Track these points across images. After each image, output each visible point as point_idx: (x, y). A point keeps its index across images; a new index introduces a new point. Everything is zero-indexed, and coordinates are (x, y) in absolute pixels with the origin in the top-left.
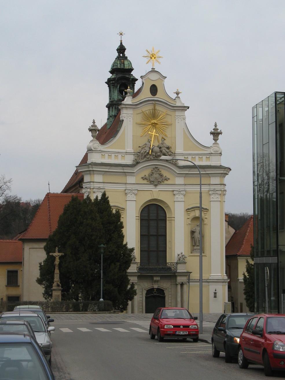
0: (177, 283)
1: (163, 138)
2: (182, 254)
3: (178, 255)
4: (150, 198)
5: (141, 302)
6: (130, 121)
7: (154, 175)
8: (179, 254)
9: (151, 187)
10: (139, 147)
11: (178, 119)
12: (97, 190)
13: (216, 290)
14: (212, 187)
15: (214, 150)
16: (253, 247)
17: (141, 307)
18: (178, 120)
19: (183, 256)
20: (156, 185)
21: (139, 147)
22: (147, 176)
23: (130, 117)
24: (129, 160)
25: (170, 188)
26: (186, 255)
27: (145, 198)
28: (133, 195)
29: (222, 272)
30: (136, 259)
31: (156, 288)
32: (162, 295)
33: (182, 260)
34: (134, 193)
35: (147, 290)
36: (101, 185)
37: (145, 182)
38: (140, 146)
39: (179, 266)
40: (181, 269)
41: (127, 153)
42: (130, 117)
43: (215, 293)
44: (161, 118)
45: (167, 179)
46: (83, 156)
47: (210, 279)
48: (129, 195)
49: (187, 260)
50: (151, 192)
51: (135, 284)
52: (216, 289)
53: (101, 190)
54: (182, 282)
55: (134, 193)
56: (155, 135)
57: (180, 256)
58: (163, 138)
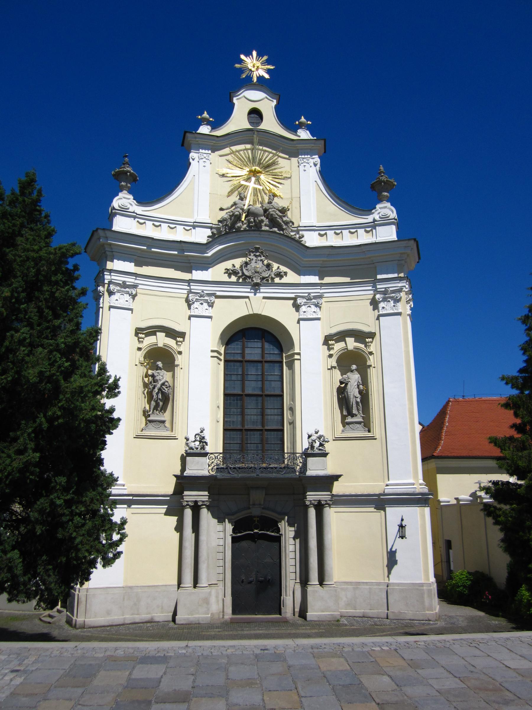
0: (185, 503)
1: (209, 466)
2: (317, 433)
3: (309, 437)
4: (244, 312)
5: (221, 549)
6: (204, 166)
7: (251, 264)
8: (310, 434)
9: (245, 290)
10: (221, 209)
11: (305, 164)
12: (119, 288)
13: (402, 520)
14: (195, 288)
15: (380, 215)
16: (55, 637)
17: (221, 563)
18: (304, 166)
19: (319, 438)
20: (256, 287)
21: (221, 209)
22: (238, 266)
23: (204, 160)
24: (201, 236)
25: (290, 293)
26: (329, 436)
27: (231, 310)
28: (205, 305)
29: (416, 477)
30: (207, 445)
31: (258, 517)
32: (272, 532)
33: (316, 451)
34: (206, 301)
35: (234, 521)
36: (130, 280)
37: (234, 279)
38: (224, 207)
39: (311, 461)
40: (315, 468)
41: (195, 225)
42: (204, 160)
43: (402, 527)
44: (266, 157)
45: (279, 275)
46: (126, 262)
47: (387, 491)
48: (196, 305)
49: (328, 447)
50: (247, 300)
51: (202, 505)
52: (403, 518)
53: (127, 290)
54: (319, 501)
55: (206, 301)
56: (255, 189)
57: (314, 437)
58: (209, 466)
